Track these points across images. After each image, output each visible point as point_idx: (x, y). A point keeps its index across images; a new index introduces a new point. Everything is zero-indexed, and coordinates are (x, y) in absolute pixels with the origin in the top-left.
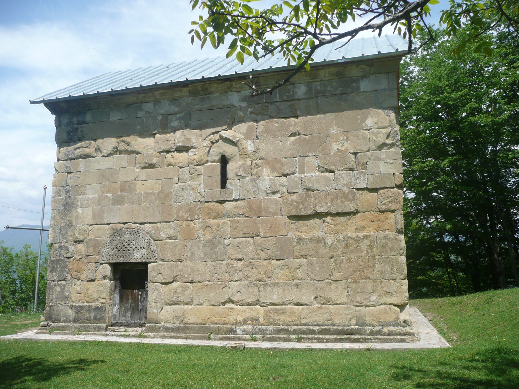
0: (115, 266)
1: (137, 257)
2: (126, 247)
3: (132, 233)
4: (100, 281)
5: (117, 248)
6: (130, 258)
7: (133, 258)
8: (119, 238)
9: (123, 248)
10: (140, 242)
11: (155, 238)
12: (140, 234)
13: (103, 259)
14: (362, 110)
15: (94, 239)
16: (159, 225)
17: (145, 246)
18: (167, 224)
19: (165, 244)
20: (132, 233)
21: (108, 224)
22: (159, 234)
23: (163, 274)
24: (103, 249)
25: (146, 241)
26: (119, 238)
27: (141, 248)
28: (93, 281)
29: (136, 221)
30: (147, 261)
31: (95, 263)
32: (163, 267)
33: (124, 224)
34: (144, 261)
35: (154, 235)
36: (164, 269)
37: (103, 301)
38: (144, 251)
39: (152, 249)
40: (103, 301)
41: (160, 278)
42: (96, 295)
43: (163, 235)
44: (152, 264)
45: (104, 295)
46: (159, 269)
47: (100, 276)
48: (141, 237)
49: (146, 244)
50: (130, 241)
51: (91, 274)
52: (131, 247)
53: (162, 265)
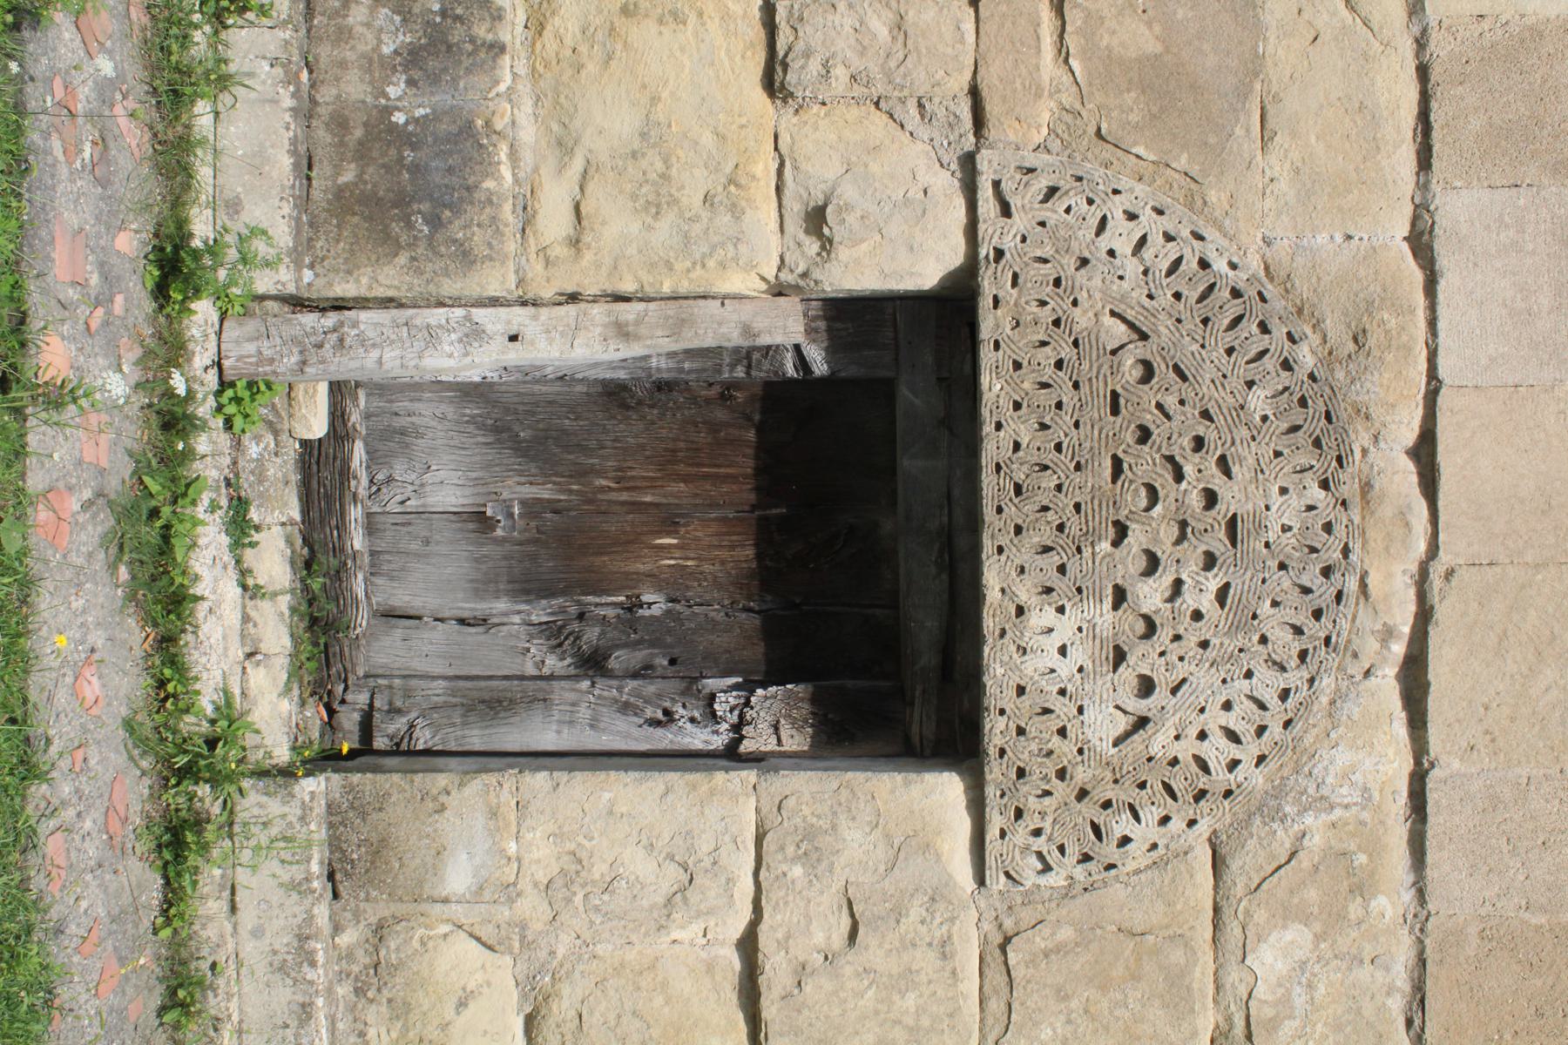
0: (951, 311)
1: (1038, 644)
2: (1152, 564)
3: (1311, 577)
4: (765, 166)
5: (1148, 372)
6: (1023, 552)
7: (1025, 592)
8: (1258, 401)
9: (1145, 464)
10: (1204, 679)
11: (1243, 867)
12: (1296, 677)
13: (1024, 199)
14: (1428, 684)
15: (1255, 66)
16: (1391, 902)
17: (1159, 741)
18: (1396, 1006)
19: (1177, 981)
20: (1311, 577)
21: (1421, 244)
22: (1288, 914)
23: (851, 964)
24: (1138, 194)
25: (1217, 750)
26: (1258, 401)
27: (1146, 687)
28: (773, 83)
29: (1443, 612)
30: (996, 773)
31: (974, 93)
32: (925, 960)
33: (1425, 452)
34: (996, 731)
35: (1283, 840)
36: (907, 979)
37: (554, 222)
38: (1102, 725)
39: (1121, 825)
40: (554, 222)
41: (802, 928)
42: (610, 120)
43: (1275, 956)
44: (963, 825)
45: (617, 224)
46: (898, 914)
47: (820, 168)
48: (1267, 683)
49: (1186, 750)
50: (1218, 541)
51: (844, 46)
52: (1152, 564)
53: (945, 949)
